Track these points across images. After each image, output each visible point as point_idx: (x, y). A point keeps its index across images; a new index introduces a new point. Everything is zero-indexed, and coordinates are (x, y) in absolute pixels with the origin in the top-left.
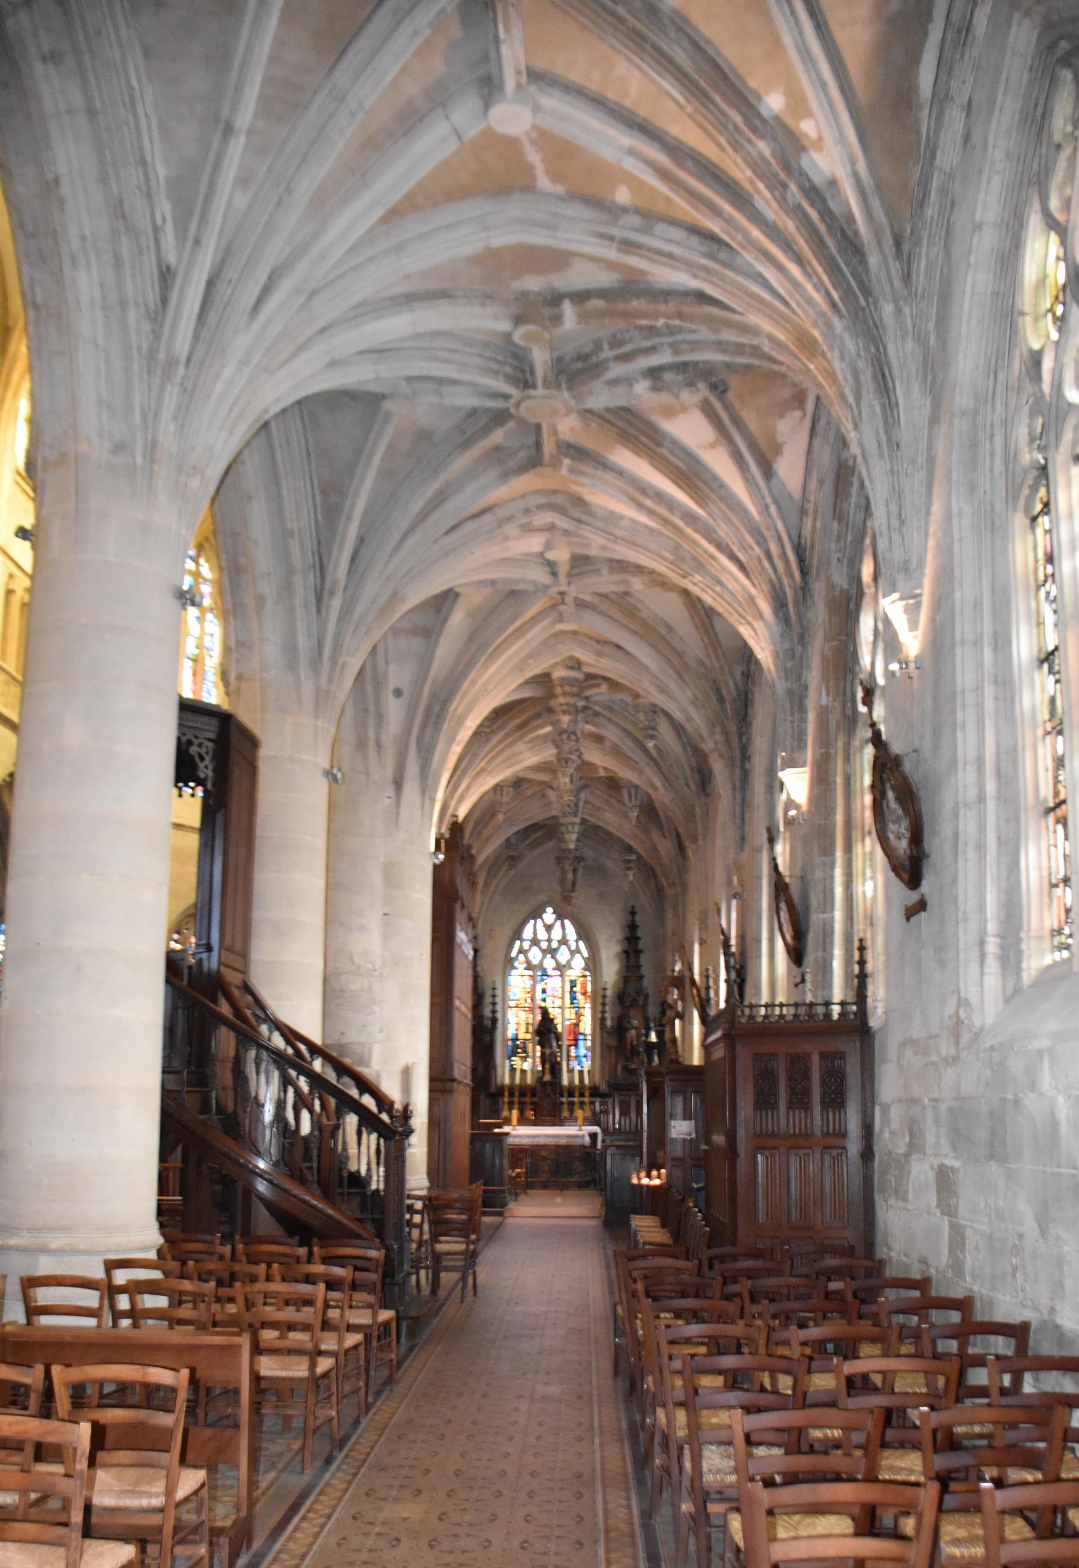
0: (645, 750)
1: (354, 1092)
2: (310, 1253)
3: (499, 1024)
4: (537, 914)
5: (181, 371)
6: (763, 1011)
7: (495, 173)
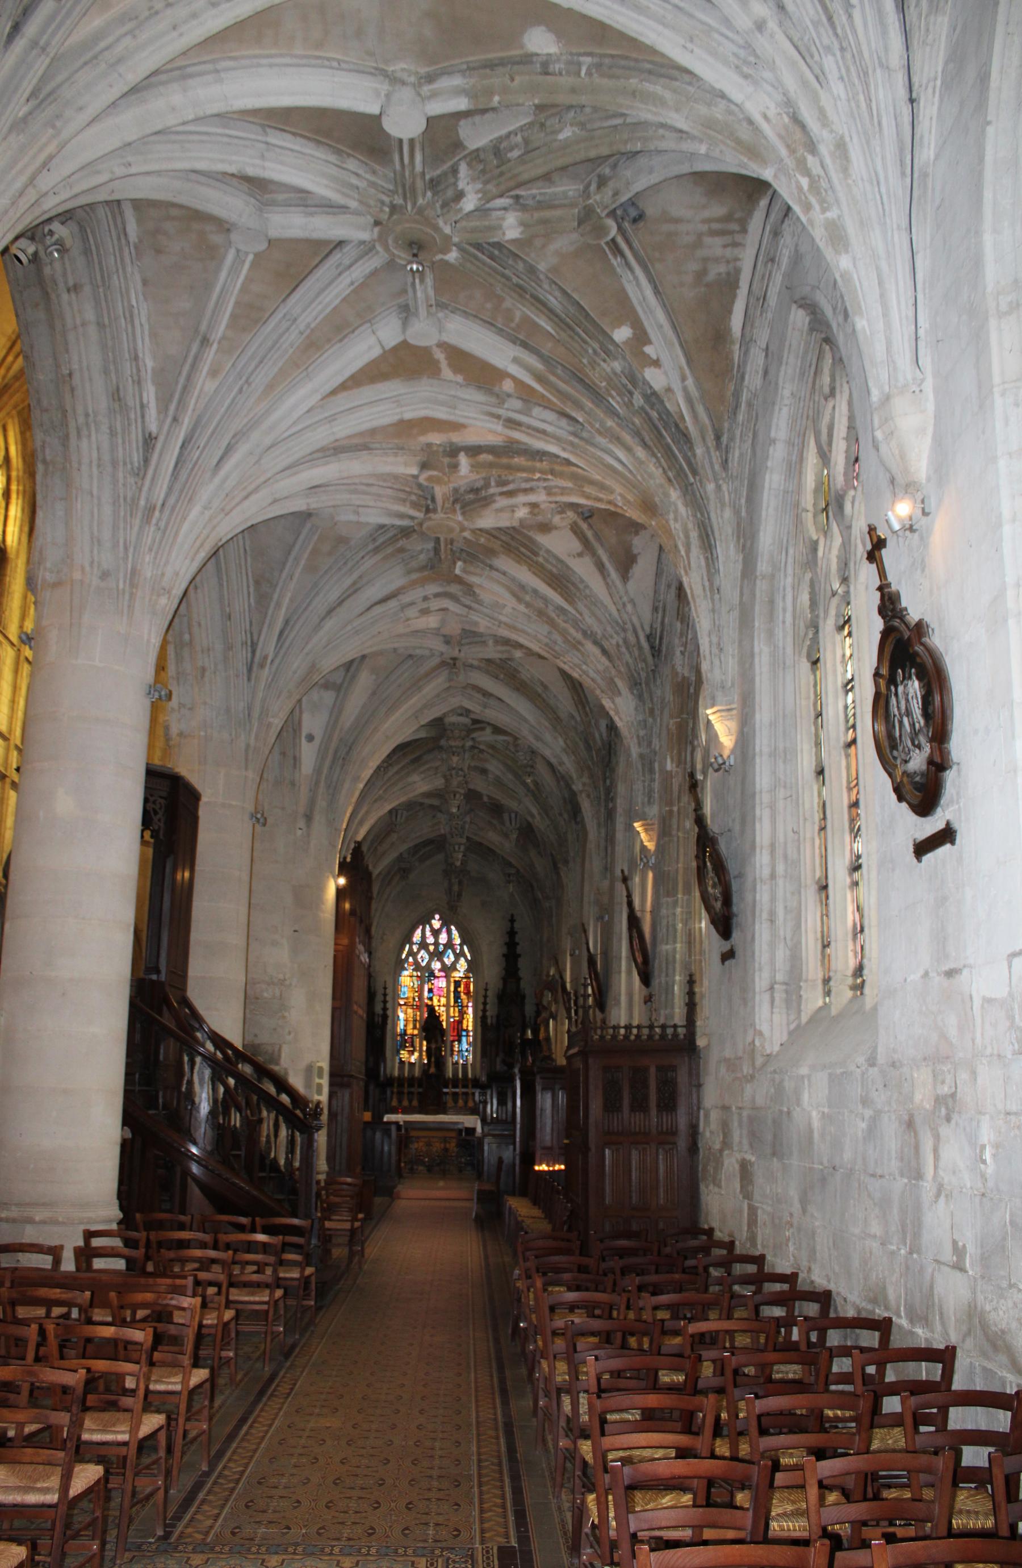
0: (524, 784)
1: (272, 1090)
2: (253, 1223)
3: (389, 1021)
4: (426, 920)
5: (157, 514)
6: (611, 1031)
7: (406, 363)
